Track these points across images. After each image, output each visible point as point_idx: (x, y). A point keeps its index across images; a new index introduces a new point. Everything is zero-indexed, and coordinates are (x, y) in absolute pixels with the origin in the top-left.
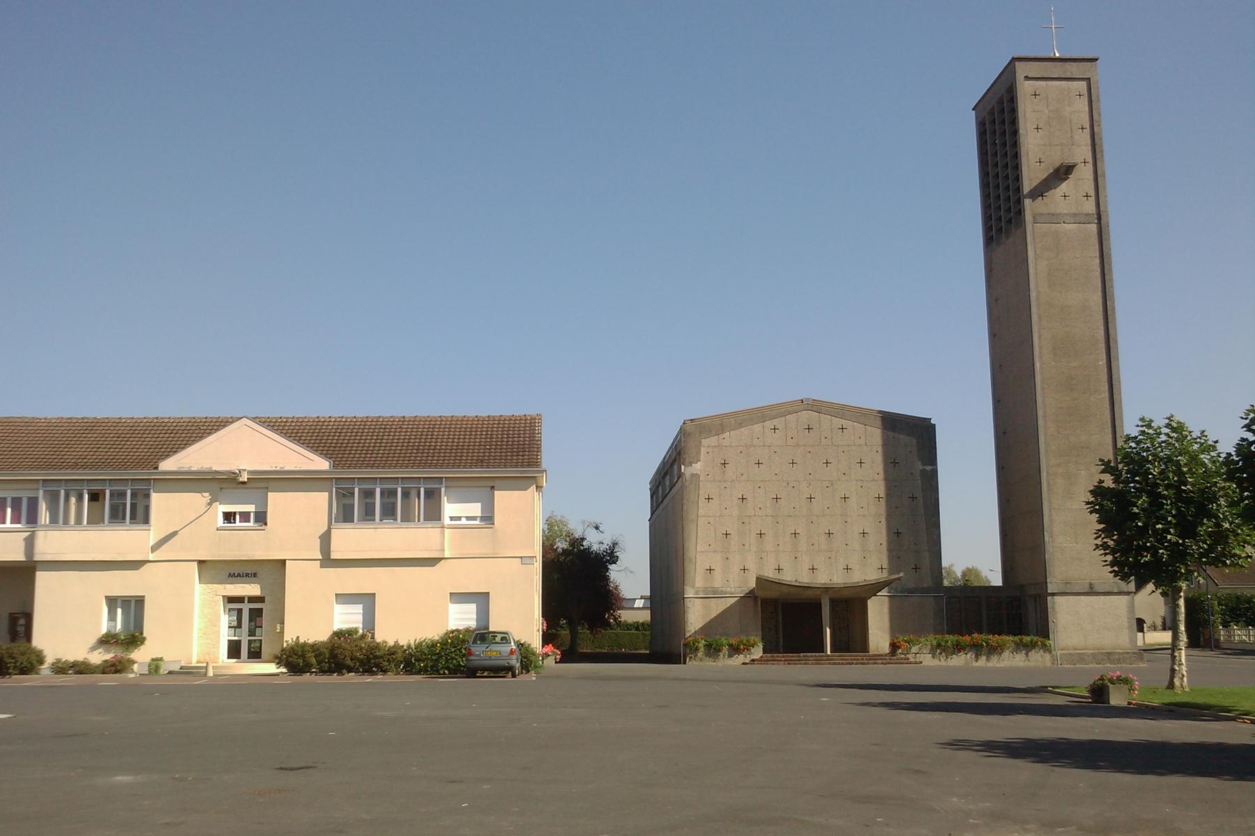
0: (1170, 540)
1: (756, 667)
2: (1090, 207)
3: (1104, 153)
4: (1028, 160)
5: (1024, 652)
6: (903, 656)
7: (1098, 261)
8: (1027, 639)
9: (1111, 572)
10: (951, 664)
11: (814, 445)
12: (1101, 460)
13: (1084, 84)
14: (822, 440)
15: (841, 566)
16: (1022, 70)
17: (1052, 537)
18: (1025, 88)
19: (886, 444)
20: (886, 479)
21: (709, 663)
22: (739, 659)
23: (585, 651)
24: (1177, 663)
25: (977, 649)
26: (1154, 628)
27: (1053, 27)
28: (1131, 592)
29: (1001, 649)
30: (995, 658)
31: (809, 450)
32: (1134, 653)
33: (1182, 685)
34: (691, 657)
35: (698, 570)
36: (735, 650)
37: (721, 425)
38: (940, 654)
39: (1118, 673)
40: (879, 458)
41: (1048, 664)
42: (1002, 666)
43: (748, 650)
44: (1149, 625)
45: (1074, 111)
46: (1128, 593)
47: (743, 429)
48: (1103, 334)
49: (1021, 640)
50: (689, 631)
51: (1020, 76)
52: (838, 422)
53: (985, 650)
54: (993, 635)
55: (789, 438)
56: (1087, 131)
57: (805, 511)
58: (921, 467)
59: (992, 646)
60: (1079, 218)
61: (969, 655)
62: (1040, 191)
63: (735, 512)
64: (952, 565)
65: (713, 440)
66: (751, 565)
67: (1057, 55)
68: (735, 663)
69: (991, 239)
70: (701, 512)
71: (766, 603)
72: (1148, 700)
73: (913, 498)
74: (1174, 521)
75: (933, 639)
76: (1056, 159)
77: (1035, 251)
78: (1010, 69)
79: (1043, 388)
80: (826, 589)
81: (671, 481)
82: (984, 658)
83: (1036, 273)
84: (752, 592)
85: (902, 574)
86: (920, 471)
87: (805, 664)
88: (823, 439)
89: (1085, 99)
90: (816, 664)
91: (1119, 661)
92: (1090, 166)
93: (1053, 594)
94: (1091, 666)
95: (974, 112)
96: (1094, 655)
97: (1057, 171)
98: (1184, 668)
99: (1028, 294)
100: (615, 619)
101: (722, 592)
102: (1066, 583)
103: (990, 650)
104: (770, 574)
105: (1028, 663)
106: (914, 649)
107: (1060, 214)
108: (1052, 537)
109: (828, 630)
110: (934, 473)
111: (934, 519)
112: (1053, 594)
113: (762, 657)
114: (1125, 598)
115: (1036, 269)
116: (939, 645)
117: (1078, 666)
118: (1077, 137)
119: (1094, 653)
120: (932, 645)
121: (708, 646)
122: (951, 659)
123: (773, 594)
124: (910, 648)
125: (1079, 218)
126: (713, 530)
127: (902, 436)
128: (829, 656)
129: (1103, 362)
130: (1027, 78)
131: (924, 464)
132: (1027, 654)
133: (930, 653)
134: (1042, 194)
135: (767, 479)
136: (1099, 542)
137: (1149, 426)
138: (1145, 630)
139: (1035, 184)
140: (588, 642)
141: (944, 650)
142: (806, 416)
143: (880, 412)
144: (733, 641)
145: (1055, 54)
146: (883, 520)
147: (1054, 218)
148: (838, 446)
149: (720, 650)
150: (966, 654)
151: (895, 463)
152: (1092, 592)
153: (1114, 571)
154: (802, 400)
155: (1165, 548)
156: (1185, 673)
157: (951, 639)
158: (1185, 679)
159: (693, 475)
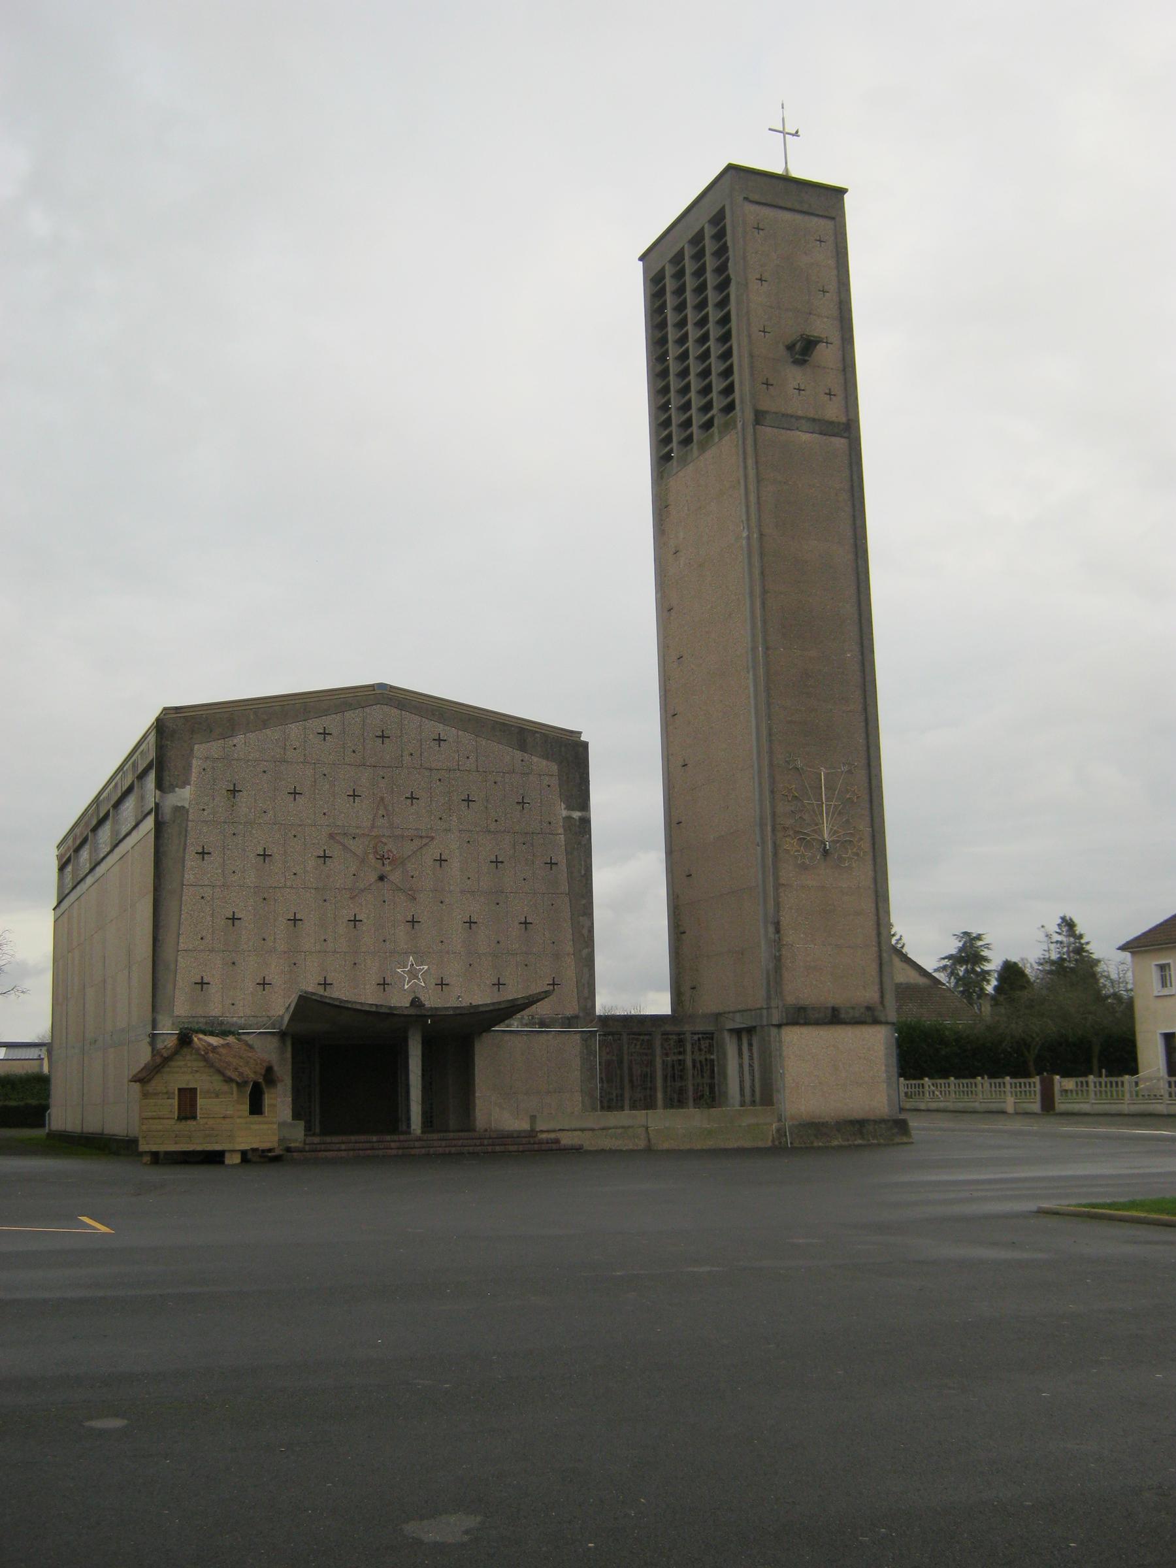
35: (180, 983)
47: (268, 731)
58: (565, 813)
65: (214, 748)
66: (275, 971)
70: (189, 877)
81: (115, 832)
86: (564, 818)
110: (585, 823)
111: (584, 902)
127: (535, 759)
131: (569, 808)
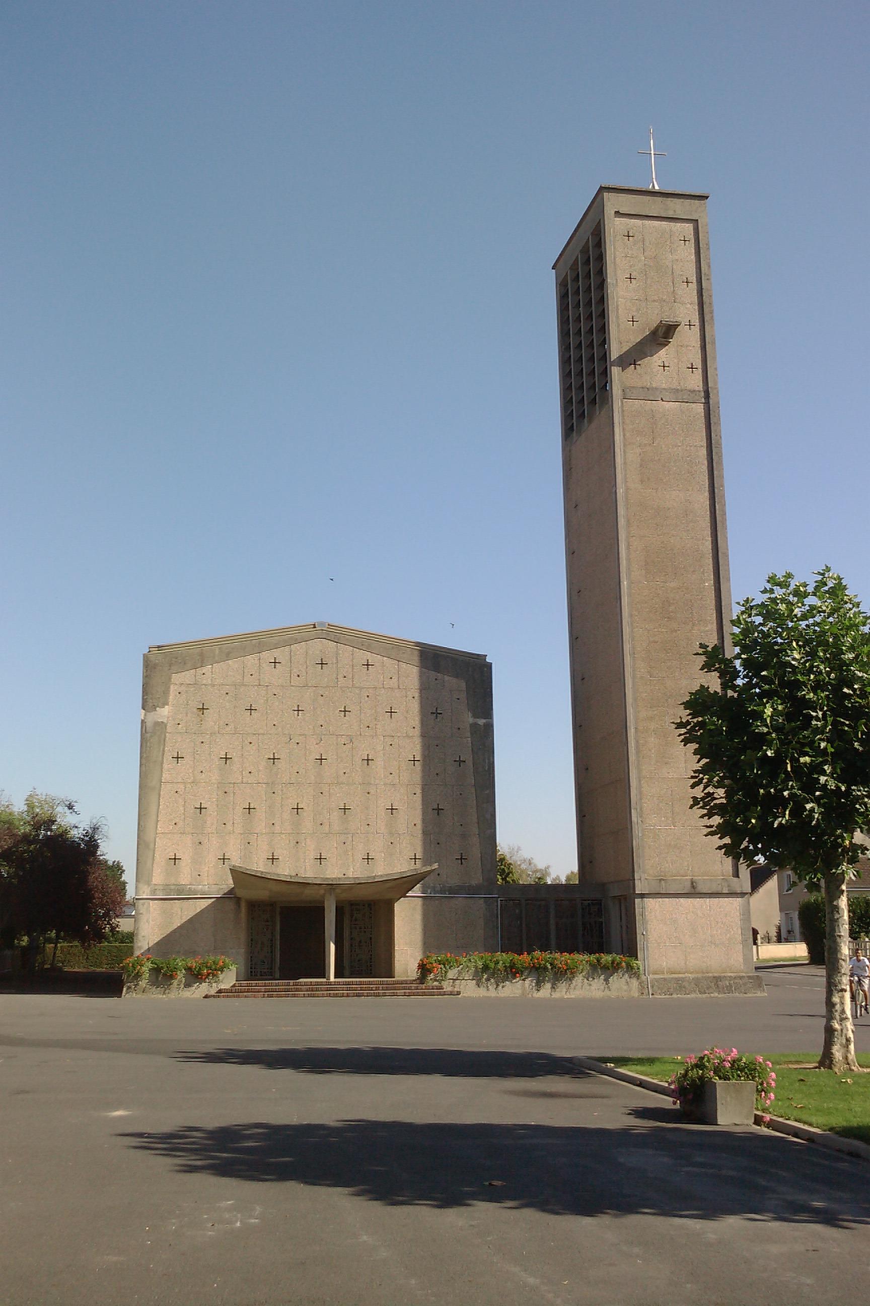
0: (825, 785)
1: (221, 1001)
2: (695, 381)
3: (715, 314)
4: (617, 317)
5: (602, 977)
6: (436, 983)
7: (704, 451)
8: (606, 958)
9: (720, 848)
10: (503, 995)
11: (327, 687)
12: (702, 646)
13: (690, 227)
14: (339, 680)
15: (360, 855)
16: (612, 203)
17: (641, 817)
18: (614, 227)
19: (424, 688)
20: (423, 735)
21: (156, 995)
22: (203, 988)
23: (76, 970)
24: (838, 1017)
25: (538, 972)
26: (769, 940)
27: (652, 152)
28: (747, 893)
29: (572, 973)
30: (562, 986)
31: (321, 693)
32: (749, 977)
33: (846, 1058)
34: (129, 988)
36: (195, 976)
37: (201, 655)
38: (488, 980)
39: (735, 1053)
40: (415, 706)
41: (635, 993)
42: (573, 996)
43: (214, 975)
44: (762, 936)
45: (677, 260)
46: (743, 895)
48: (710, 547)
49: (598, 961)
50: (140, 948)
51: (609, 211)
52: (363, 656)
53: (549, 974)
54: (561, 953)
55: (294, 677)
56: (694, 286)
57: (313, 778)
59: (560, 968)
60: (680, 395)
61: (527, 982)
62: (631, 359)
63: (215, 777)
64: (548, 867)
65: (187, 676)
67: (657, 187)
68: (194, 996)
69: (570, 429)
70: (166, 776)
71: (253, 906)
72: (796, 1113)
73: (460, 762)
74: (831, 750)
75: (477, 959)
76: (653, 318)
77: (624, 435)
78: (596, 206)
79: (631, 616)
80: (332, 887)
82: (548, 986)
83: (625, 463)
84: (231, 891)
85: (436, 866)
87: (294, 996)
88: (341, 679)
89: (692, 246)
90: (309, 996)
91: (729, 989)
92: (696, 330)
93: (642, 896)
94: (693, 996)
95: (554, 271)
96: (697, 981)
97: (654, 333)
98: (849, 1025)
99: (614, 490)
100: (113, 929)
101: (190, 891)
102: (660, 880)
103: (556, 974)
104: (258, 865)
105: (607, 992)
106: (452, 974)
107: (656, 389)
108: (641, 817)
109: (333, 947)
110: (489, 728)
111: (487, 792)
112: (642, 896)
113: (234, 986)
114: (737, 902)
115: (625, 459)
116: (486, 968)
117: (675, 996)
118: (680, 292)
119: (698, 978)
120: (476, 967)
121: (156, 971)
122: (503, 987)
123: (261, 894)
124: (446, 972)
125: (680, 395)
126: (181, 802)
127: (447, 678)
128: (330, 984)
129: (709, 583)
130: (617, 213)
131: (475, 716)
132: (606, 980)
133: (473, 979)
134: (635, 362)
135: (261, 731)
136: (699, 792)
137: (783, 585)
138: (759, 941)
139: (625, 349)
140: (81, 958)
141: (493, 975)
142: (318, 647)
143: (418, 644)
144: (192, 963)
145: (653, 186)
146: (419, 791)
147: (650, 394)
148: (361, 688)
149: (172, 977)
150: (524, 980)
151: (437, 714)
152: (693, 892)
153: (725, 846)
154: (314, 625)
155: (817, 800)
156: (851, 1035)
157: (503, 958)
158: (852, 1047)
159: (157, 724)
